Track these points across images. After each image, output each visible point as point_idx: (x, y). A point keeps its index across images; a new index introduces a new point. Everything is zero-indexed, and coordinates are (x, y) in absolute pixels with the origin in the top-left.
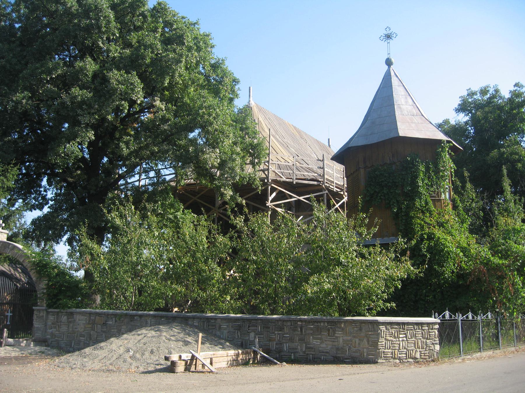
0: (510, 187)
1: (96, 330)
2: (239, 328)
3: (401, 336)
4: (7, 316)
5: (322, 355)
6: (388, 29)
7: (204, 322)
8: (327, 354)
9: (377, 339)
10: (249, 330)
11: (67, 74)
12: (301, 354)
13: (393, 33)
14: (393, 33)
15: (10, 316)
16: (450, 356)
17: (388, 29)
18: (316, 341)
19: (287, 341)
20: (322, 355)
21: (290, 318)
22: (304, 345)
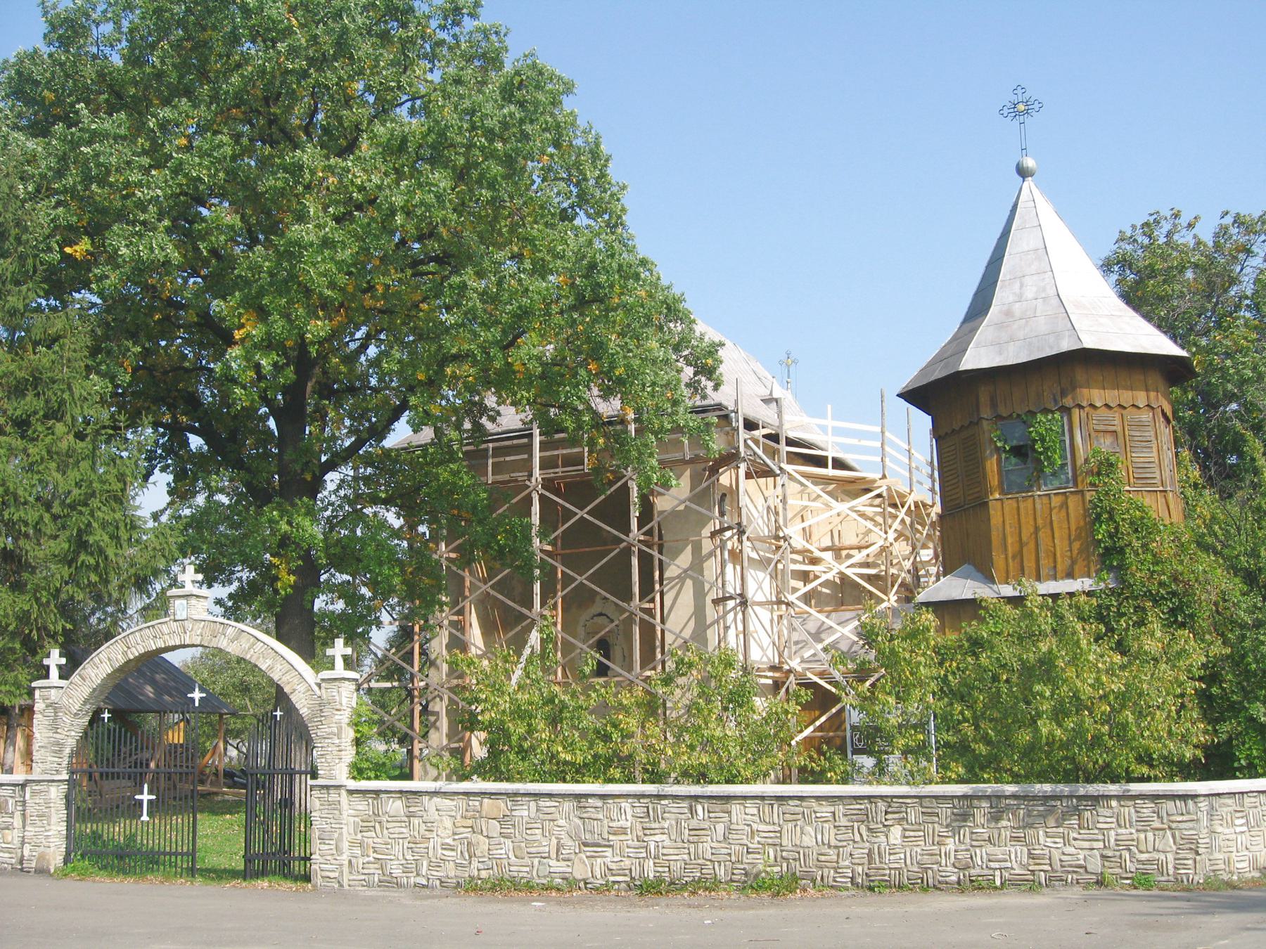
0: (13, 446)
1: (485, 834)
2: (865, 817)
3: (1238, 822)
4: (141, 801)
5: (1069, 872)
6: (1019, 91)
7: (772, 805)
8: (1081, 870)
9: (907, 834)
10: (886, 820)
11: (422, 229)
12: (1016, 872)
13: (1032, 100)
14: (1032, 100)
15: (150, 802)
16: (83, 875)
17: (1019, 91)
18: (1053, 840)
19: (983, 843)
20: (1069, 872)
21: (1129, 791)
22: (1025, 849)
